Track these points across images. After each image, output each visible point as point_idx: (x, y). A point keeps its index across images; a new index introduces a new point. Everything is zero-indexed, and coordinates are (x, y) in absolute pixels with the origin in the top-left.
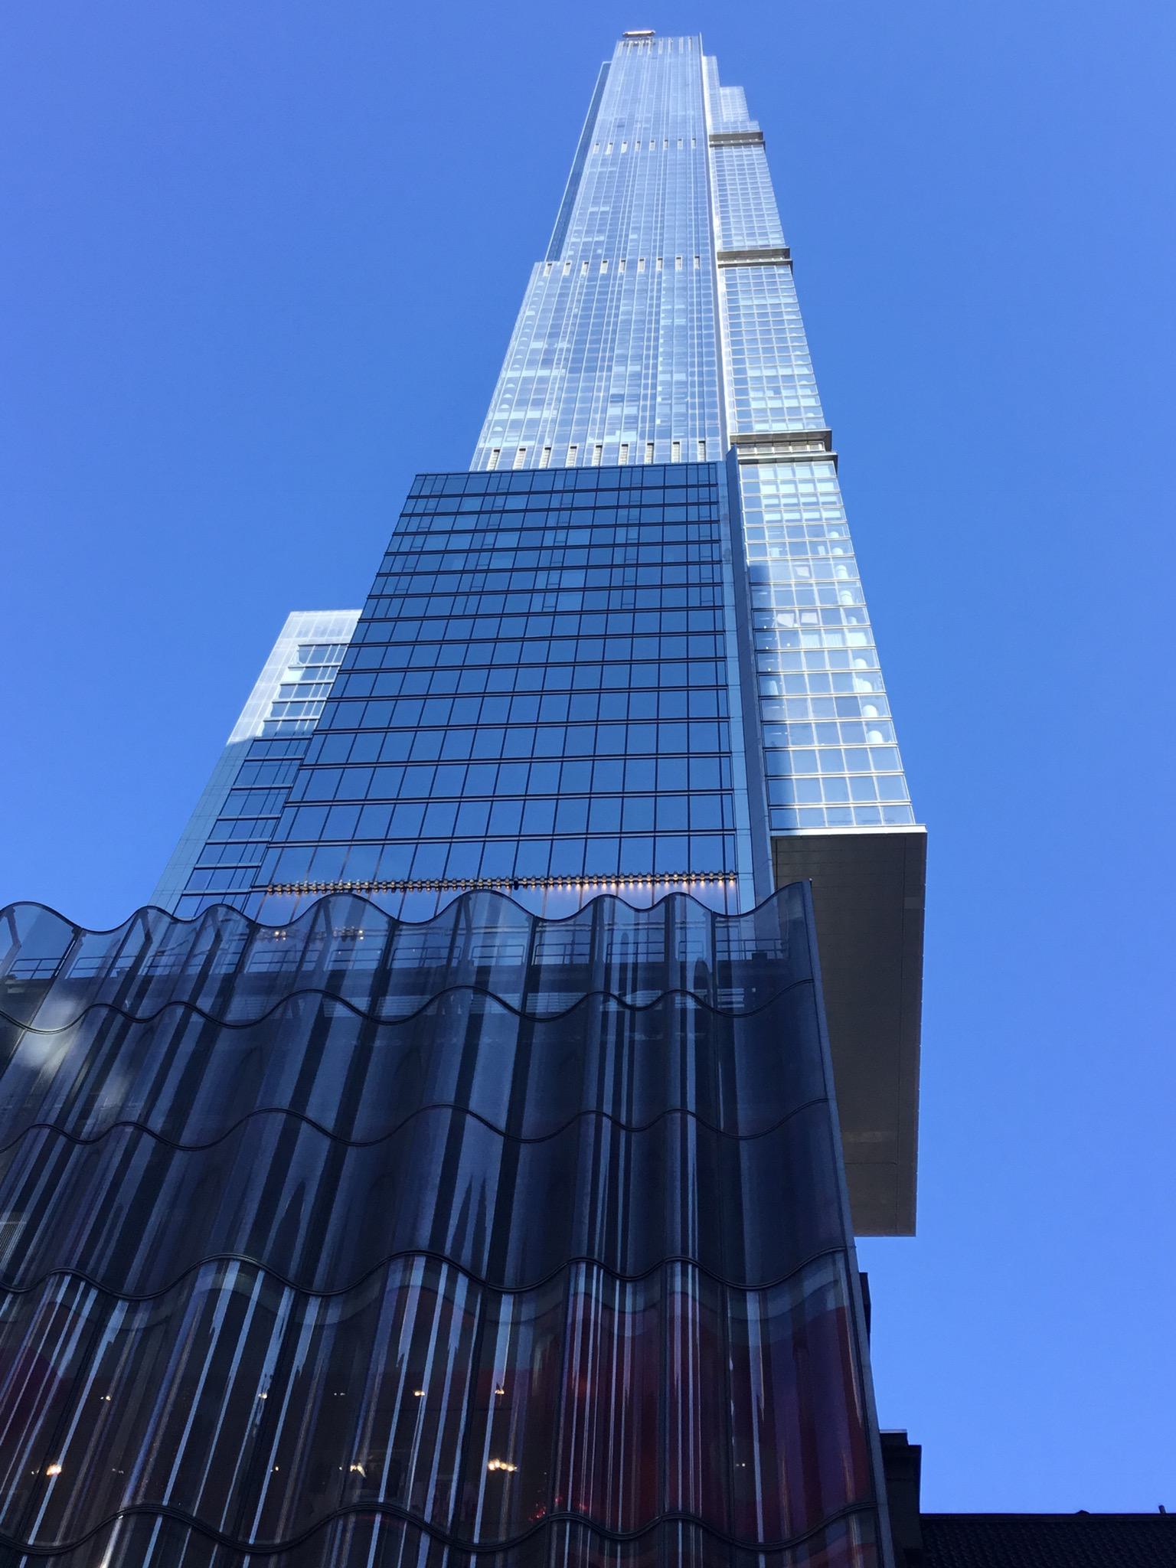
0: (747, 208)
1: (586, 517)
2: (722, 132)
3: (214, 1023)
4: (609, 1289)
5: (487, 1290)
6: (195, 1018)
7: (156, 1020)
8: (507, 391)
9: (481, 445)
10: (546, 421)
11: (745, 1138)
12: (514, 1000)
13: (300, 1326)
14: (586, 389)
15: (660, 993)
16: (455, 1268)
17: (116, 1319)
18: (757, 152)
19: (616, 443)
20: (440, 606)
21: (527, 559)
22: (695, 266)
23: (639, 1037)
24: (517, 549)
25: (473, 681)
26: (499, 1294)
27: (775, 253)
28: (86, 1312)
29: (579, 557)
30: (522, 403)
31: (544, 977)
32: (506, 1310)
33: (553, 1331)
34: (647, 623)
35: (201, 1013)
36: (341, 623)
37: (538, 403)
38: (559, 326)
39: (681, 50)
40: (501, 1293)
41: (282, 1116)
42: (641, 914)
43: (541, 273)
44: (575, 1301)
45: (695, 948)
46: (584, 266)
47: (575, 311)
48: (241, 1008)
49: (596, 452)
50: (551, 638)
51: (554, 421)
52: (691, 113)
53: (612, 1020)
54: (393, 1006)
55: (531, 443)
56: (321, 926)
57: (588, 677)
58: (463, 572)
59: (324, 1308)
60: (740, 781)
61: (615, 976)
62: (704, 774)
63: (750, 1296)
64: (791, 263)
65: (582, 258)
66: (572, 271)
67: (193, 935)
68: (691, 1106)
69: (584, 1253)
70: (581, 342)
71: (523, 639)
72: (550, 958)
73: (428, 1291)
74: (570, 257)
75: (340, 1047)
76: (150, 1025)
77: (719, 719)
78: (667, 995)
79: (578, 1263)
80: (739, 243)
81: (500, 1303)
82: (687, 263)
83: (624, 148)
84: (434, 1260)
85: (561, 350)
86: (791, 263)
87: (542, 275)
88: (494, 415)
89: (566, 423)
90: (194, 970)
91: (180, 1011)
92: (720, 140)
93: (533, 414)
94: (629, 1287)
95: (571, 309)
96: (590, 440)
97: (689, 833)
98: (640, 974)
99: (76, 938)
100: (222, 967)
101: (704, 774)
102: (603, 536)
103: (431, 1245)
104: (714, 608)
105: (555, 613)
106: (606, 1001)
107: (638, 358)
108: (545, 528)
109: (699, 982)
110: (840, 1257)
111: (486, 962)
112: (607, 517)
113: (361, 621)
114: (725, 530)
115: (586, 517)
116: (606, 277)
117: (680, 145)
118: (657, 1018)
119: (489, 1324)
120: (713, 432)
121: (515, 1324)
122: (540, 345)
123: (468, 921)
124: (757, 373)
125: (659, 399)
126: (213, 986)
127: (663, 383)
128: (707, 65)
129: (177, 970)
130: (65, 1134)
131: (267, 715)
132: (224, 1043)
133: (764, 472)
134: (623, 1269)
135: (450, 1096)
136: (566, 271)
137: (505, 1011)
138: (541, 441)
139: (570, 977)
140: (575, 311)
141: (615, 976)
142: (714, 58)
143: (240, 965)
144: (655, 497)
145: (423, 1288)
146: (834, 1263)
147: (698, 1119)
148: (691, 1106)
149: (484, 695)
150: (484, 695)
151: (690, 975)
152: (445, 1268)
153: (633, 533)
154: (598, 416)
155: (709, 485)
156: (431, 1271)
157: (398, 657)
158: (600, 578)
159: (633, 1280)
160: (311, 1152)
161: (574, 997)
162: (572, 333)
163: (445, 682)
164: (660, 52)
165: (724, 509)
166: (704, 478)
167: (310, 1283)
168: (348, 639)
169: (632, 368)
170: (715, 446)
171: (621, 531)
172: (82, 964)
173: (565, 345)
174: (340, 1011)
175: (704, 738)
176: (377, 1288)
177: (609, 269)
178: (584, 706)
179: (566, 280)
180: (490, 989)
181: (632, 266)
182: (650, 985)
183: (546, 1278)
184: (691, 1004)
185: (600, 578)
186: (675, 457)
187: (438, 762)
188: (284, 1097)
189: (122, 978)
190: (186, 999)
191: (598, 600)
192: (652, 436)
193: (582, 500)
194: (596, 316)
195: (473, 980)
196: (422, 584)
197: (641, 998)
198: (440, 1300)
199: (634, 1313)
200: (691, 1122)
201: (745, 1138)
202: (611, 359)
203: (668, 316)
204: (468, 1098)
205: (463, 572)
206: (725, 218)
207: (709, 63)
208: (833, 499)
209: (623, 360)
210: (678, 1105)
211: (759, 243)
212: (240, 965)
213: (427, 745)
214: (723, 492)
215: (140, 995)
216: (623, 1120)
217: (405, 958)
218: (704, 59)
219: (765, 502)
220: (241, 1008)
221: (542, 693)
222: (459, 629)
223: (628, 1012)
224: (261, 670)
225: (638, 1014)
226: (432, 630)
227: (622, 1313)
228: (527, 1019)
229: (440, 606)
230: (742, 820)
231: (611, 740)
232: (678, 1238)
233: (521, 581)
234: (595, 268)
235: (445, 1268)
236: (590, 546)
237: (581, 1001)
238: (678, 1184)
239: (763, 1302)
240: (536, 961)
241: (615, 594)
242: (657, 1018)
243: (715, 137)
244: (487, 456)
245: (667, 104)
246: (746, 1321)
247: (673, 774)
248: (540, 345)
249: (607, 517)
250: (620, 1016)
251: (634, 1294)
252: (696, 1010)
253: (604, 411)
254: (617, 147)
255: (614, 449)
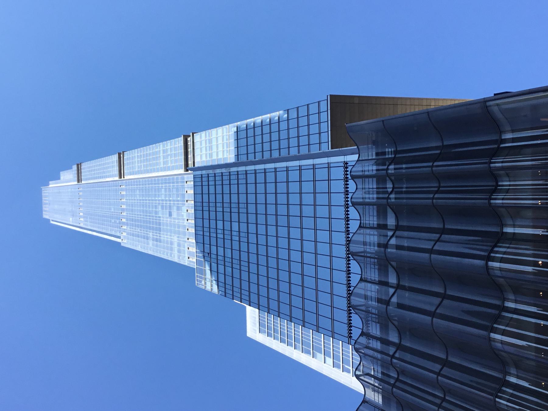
0: (102, 169)
1: (213, 223)
2: (76, 179)
3: (399, 347)
4: (501, 191)
5: (501, 238)
6: (397, 355)
7: (398, 370)
8: (167, 255)
9: (186, 264)
10: (178, 240)
11: (443, 143)
12: (392, 291)
13: (516, 309)
14: (167, 226)
15: (388, 178)
16: (492, 251)
17: (513, 380)
18: (84, 166)
19: (185, 215)
20: (245, 276)
21: (228, 244)
22: (124, 187)
23: (405, 186)
24: (224, 248)
25: (273, 263)
26: (503, 233)
27: (120, 158)
28: (511, 391)
29: (227, 225)
30: (172, 249)
31: (381, 222)
32: (509, 230)
33: (516, 212)
34: (251, 198)
35: (395, 353)
36: (252, 313)
37: (172, 243)
38: (144, 236)
39: (47, 194)
40: (504, 306)
41: (434, 319)
42: (358, 187)
43: (125, 243)
44: (506, 203)
45: (371, 168)
46: (123, 227)
47: (139, 231)
48: (394, 337)
49: (189, 221)
50: (257, 234)
51: (178, 237)
52: (69, 190)
53: (398, 196)
54: (393, 279)
55: (186, 245)
56: (363, 308)
57: (271, 220)
58: (232, 268)
59: (510, 374)
60: (310, 162)
61: (381, 196)
62: (307, 175)
63: (503, 138)
64: (123, 152)
65: (120, 228)
66: (124, 232)
67: (367, 357)
68: (431, 164)
69: (487, 201)
70: (150, 228)
71: (257, 244)
72: (373, 220)
73: (502, 260)
74: (120, 232)
75: (408, 298)
76: (401, 372)
77: (287, 171)
78: (388, 175)
79: (491, 203)
80: (117, 172)
81: (506, 232)
82: (122, 190)
83: (81, 214)
84: (489, 258)
85: (153, 235)
86: (123, 152)
87: (126, 242)
88: (176, 260)
89: (179, 233)
90: (379, 356)
91: (394, 361)
92: (79, 180)
93: (175, 245)
94: (500, 183)
95: (138, 232)
96: (185, 224)
97: (329, 180)
98: (381, 186)
99: (367, 402)
100: (377, 345)
101: (307, 175)
102: (220, 242)
103: (483, 260)
104: (246, 174)
105: (248, 233)
106: (390, 199)
107: (156, 207)
108: (217, 238)
109: (384, 164)
110: (489, 104)
111: (376, 245)
112: (213, 214)
113: (250, 305)
114: (218, 171)
115: (213, 223)
116: (127, 219)
117: (81, 194)
118: (397, 179)
119: (515, 239)
120: (183, 178)
121: (514, 226)
122: (151, 242)
123: (362, 252)
124: (162, 163)
125: (171, 199)
126: (385, 348)
127: (165, 197)
128: (53, 185)
129: (379, 362)
130: (442, 403)
131: (285, 345)
132: (407, 343)
133: (197, 159)
134: (493, 186)
135: (427, 255)
136: (124, 234)
137: (396, 295)
138: (185, 241)
139: (382, 211)
140: (139, 231)
141: (381, 196)
142: (50, 182)
143: (377, 338)
144: (206, 197)
145: (502, 335)
146: (490, 106)
147: (435, 161)
148: (431, 164)
149: (278, 258)
150: (278, 258)
151: (381, 167)
152: (492, 255)
153: (219, 205)
154: (177, 221)
155: (202, 177)
156: (494, 259)
157: (263, 291)
158: (235, 216)
159: (497, 182)
160: (449, 307)
161: (391, 270)
162: (147, 231)
163: (273, 273)
164: (47, 202)
165: (211, 172)
166: (199, 180)
167: (499, 306)
168: (257, 310)
169: (160, 209)
170: (188, 178)
171: (218, 209)
172: (376, 398)
173: (151, 234)
174: (394, 300)
175: (294, 176)
176: (503, 353)
177: (124, 218)
178: (282, 221)
179: (128, 234)
180: (387, 299)
181: (123, 210)
182: (385, 182)
183: (497, 215)
184: (392, 167)
185: (235, 216)
186: (192, 192)
187: (303, 275)
188: (427, 319)
189: (382, 384)
190: (390, 358)
191: (243, 217)
192: (184, 201)
193: (206, 224)
194: (141, 223)
195: (383, 249)
196: (237, 283)
197: (389, 185)
198: (505, 256)
199: (510, 181)
200: (435, 164)
201: (443, 143)
202: (156, 217)
203: (141, 201)
204: (428, 249)
205: (232, 268)
206: (106, 177)
207: (52, 184)
208: (207, 134)
209: (156, 213)
210: (430, 169)
211: (116, 164)
212: (377, 338)
213: (296, 279)
214: (204, 172)
215: (389, 376)
216: (436, 189)
217: (374, 275)
218: (50, 186)
219: (208, 159)
220: (394, 337)
221: (277, 237)
222: (253, 268)
223: (395, 190)
224: (269, 347)
225: (396, 186)
226: (254, 278)
227: (510, 185)
228: (398, 287)
229: (245, 276)
230: (325, 160)
231: (295, 210)
232: (482, 166)
233: (236, 246)
234: (124, 223)
235: (492, 255)
236: (223, 221)
237: (391, 208)
238: (461, 167)
239: (505, 132)
240: (375, 226)
241: (241, 211)
242: (397, 179)
243: (78, 181)
244: (190, 261)
245: (68, 202)
246: (513, 138)
247: (308, 187)
248: (151, 242)
249: (213, 214)
250: (396, 193)
251: (503, 181)
252: (394, 165)
253: (174, 219)
254: (81, 217)
255: (189, 215)
